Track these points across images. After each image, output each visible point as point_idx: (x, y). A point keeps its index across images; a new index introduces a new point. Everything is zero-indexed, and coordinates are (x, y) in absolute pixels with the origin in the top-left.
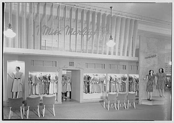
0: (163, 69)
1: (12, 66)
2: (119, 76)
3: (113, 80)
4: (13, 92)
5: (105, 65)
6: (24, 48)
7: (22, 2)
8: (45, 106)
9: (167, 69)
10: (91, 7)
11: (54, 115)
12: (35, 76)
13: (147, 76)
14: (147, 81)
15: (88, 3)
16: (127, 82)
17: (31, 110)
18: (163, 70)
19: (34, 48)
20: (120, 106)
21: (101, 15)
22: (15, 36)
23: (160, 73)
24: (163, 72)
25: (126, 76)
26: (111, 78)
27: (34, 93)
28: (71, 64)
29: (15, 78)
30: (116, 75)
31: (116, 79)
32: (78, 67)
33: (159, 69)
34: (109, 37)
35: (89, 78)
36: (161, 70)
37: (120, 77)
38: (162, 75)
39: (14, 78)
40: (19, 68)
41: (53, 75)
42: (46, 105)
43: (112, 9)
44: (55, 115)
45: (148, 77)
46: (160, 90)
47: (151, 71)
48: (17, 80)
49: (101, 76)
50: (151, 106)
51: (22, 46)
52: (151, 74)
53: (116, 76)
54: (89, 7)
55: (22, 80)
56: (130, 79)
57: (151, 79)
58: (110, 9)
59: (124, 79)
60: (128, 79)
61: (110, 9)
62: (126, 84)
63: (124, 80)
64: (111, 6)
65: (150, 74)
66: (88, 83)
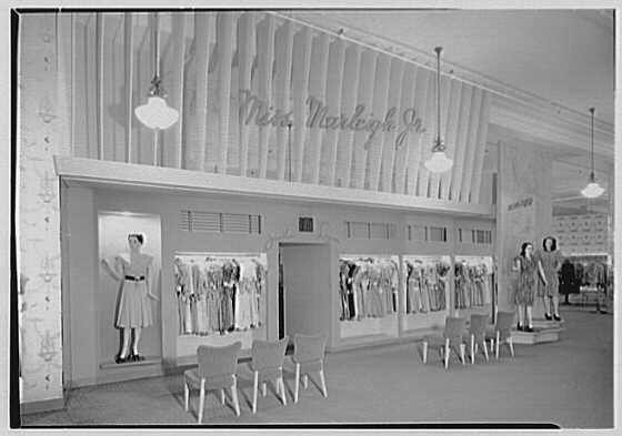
0: (557, 239)
1: (115, 229)
2: (426, 262)
3: (417, 273)
4: (122, 330)
5: (263, 219)
6: (153, 164)
7: (196, 10)
8: (203, 381)
9: (576, 235)
10: (395, 47)
11: (236, 413)
12: (196, 270)
13: (515, 260)
14: (515, 276)
15: (328, 12)
16: (448, 279)
17: (213, 391)
18: (554, 241)
19: (139, 155)
20: (301, 382)
21: (292, 34)
22: (175, 120)
23: (545, 249)
24: (553, 248)
25: (446, 260)
26: (410, 267)
27: (189, 330)
28: (306, 225)
29: (127, 278)
30: (420, 258)
31: (423, 271)
32: (323, 234)
33: (545, 241)
34: (432, 145)
35: (353, 268)
36: (548, 245)
37: (433, 265)
38: (552, 257)
39: (120, 275)
40: (140, 238)
41: (247, 269)
42: (207, 379)
43: (442, 53)
44: (296, 400)
45: (519, 262)
46: (546, 298)
47: (529, 246)
48: (136, 285)
49: (380, 263)
50: (528, 345)
51: (397, 189)
52: (527, 255)
53: (420, 262)
54: (360, 34)
55: (150, 283)
56: (458, 269)
57: (527, 268)
58: (433, 56)
59: (442, 271)
60: (452, 269)
61: (436, 54)
62: (447, 285)
63: (442, 274)
64: (438, 45)
65: (523, 253)
66: (349, 287)
